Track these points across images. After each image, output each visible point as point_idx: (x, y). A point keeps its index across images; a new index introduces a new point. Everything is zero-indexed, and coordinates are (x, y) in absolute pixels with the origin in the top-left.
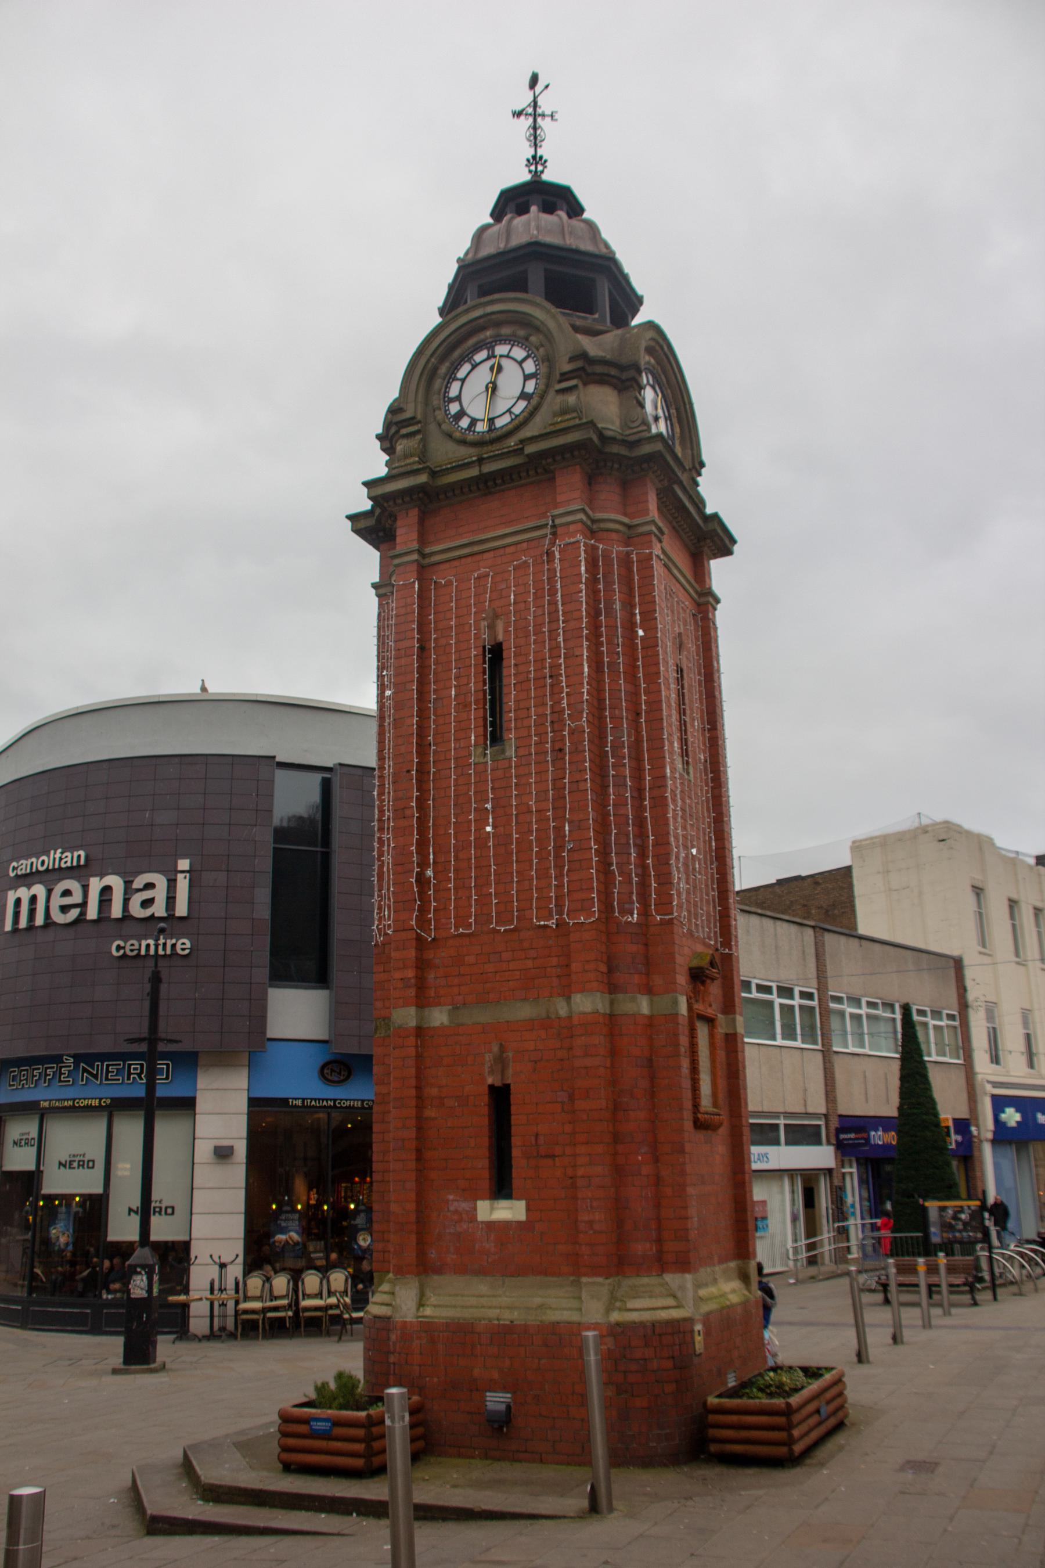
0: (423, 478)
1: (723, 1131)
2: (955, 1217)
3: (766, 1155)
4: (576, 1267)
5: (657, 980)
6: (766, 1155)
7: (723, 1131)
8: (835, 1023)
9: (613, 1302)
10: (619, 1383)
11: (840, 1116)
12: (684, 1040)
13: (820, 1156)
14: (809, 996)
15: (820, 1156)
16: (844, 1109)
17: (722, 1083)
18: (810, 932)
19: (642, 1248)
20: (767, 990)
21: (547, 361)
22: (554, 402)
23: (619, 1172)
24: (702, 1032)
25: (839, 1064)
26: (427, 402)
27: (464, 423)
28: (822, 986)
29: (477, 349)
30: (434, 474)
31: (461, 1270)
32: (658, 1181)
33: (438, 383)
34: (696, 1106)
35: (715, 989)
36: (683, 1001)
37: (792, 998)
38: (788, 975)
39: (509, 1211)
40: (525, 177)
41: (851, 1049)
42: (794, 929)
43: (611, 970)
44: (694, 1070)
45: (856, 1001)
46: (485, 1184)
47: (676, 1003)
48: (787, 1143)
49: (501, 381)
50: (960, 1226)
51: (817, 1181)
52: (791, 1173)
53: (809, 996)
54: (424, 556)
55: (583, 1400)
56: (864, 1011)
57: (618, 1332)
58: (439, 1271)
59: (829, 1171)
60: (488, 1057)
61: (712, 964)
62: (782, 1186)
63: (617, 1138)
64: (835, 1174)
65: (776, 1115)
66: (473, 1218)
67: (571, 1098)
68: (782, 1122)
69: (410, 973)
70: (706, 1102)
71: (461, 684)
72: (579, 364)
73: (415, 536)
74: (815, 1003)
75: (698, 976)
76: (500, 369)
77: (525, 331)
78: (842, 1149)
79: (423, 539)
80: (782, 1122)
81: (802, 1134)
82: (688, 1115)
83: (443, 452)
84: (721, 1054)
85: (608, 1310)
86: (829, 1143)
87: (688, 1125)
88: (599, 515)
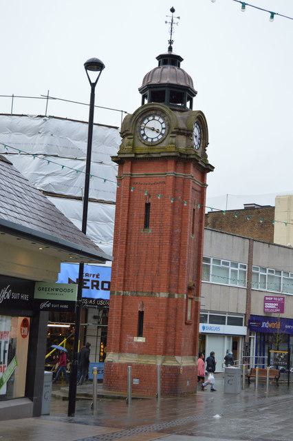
0: (133, 155)
1: (192, 325)
2: (279, 357)
3: (219, 328)
4: (156, 353)
5: (180, 290)
6: (219, 328)
7: (192, 325)
8: (254, 278)
9: (164, 361)
10: (163, 374)
11: (251, 315)
12: (185, 305)
13: (241, 330)
14: (245, 267)
15: (241, 330)
16: (254, 312)
17: (193, 314)
18: (248, 241)
19: (170, 350)
20: (227, 264)
21: (169, 125)
22: (169, 139)
23: (167, 333)
24: (190, 302)
25: (253, 295)
26: (135, 129)
27: (145, 137)
28: (250, 263)
29: (150, 116)
30: (136, 154)
31: (129, 352)
32: (175, 336)
33: (138, 124)
34: (186, 319)
35: (194, 292)
36: (185, 295)
37: (237, 267)
38: (236, 259)
39: (141, 340)
40: (165, 51)
41: (259, 289)
42: (241, 240)
43: (169, 287)
44: (187, 311)
45: (264, 270)
46: (136, 334)
47: (183, 296)
48: (228, 324)
49: (154, 132)
50: (280, 360)
51: (239, 340)
52: (229, 336)
53: (245, 267)
54: (131, 175)
55: (156, 381)
56: (267, 274)
57: (164, 367)
58: (124, 352)
59: (244, 336)
60: (139, 305)
61: (194, 285)
62: (224, 343)
63: (167, 325)
64: (246, 337)
65: (225, 313)
66: (133, 341)
67: (158, 315)
68: (227, 316)
69: (122, 283)
70: (189, 318)
71: (139, 213)
72: (177, 130)
73: (129, 169)
74: (246, 270)
75: (190, 289)
76: (157, 132)
77: (162, 114)
78: (251, 329)
79: (131, 171)
80: (227, 316)
81: (235, 321)
82: (184, 322)
83: (141, 148)
84: (194, 307)
85: (163, 362)
86: (245, 325)
87: (184, 324)
88: (178, 173)
